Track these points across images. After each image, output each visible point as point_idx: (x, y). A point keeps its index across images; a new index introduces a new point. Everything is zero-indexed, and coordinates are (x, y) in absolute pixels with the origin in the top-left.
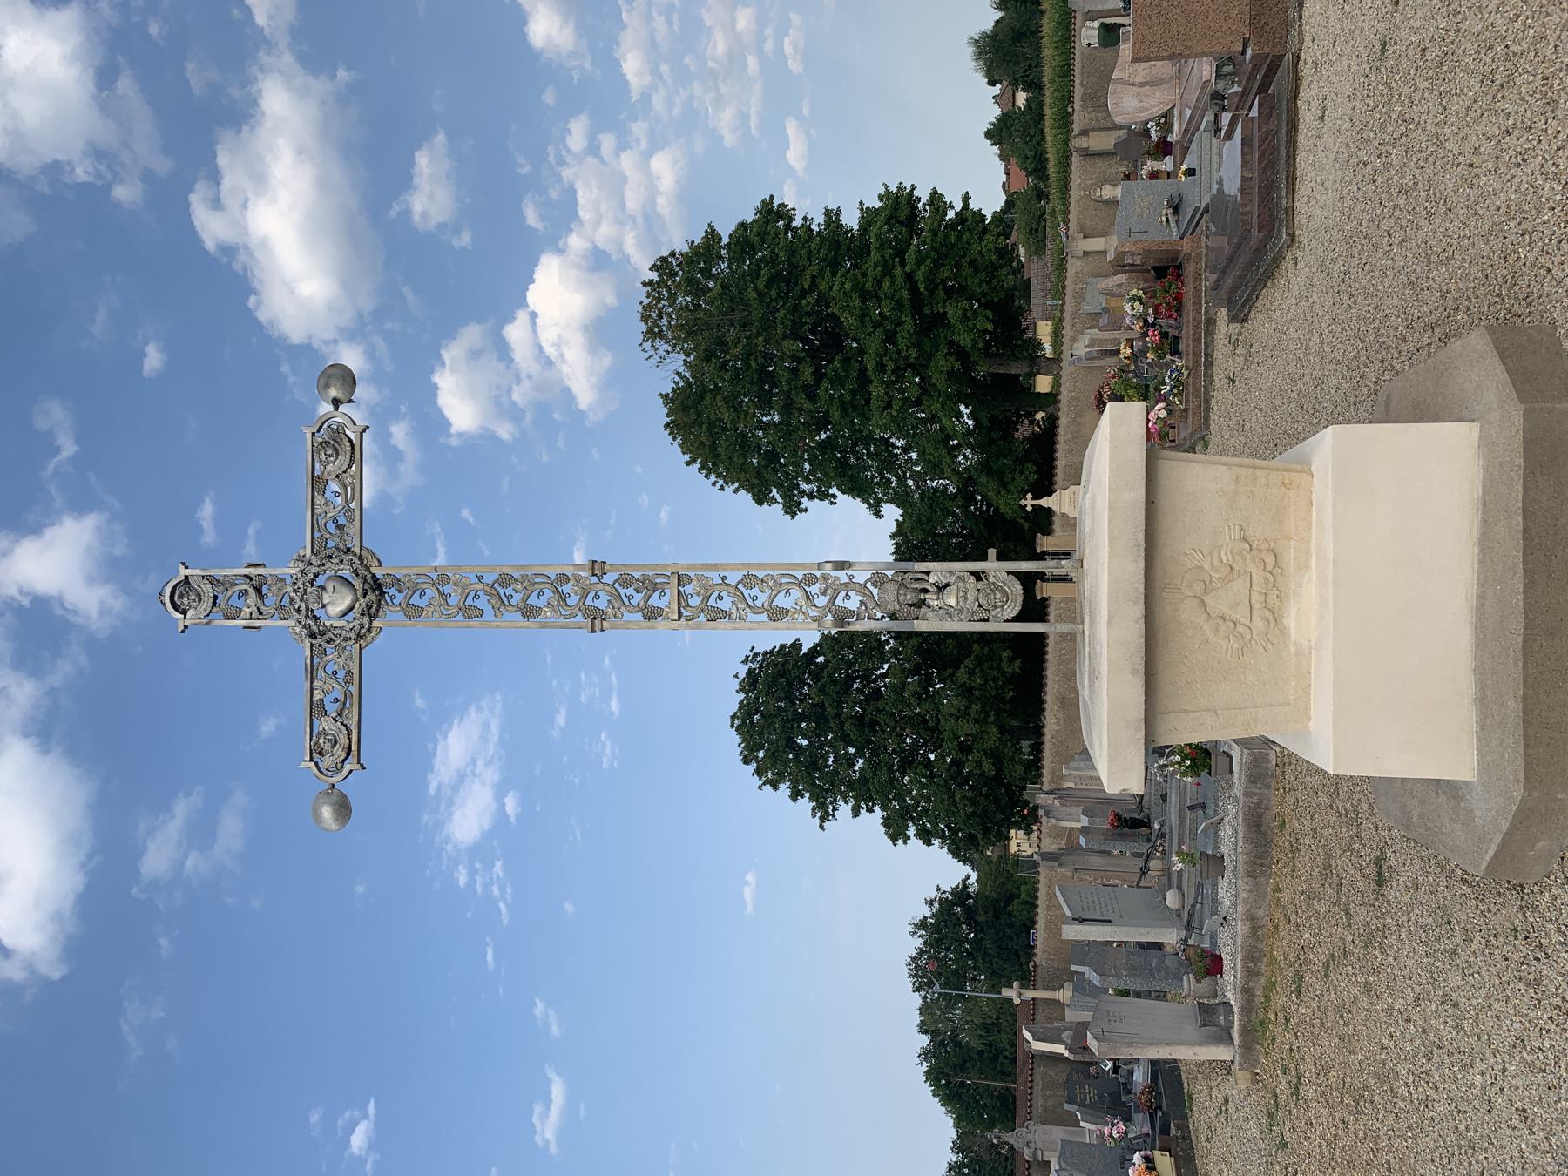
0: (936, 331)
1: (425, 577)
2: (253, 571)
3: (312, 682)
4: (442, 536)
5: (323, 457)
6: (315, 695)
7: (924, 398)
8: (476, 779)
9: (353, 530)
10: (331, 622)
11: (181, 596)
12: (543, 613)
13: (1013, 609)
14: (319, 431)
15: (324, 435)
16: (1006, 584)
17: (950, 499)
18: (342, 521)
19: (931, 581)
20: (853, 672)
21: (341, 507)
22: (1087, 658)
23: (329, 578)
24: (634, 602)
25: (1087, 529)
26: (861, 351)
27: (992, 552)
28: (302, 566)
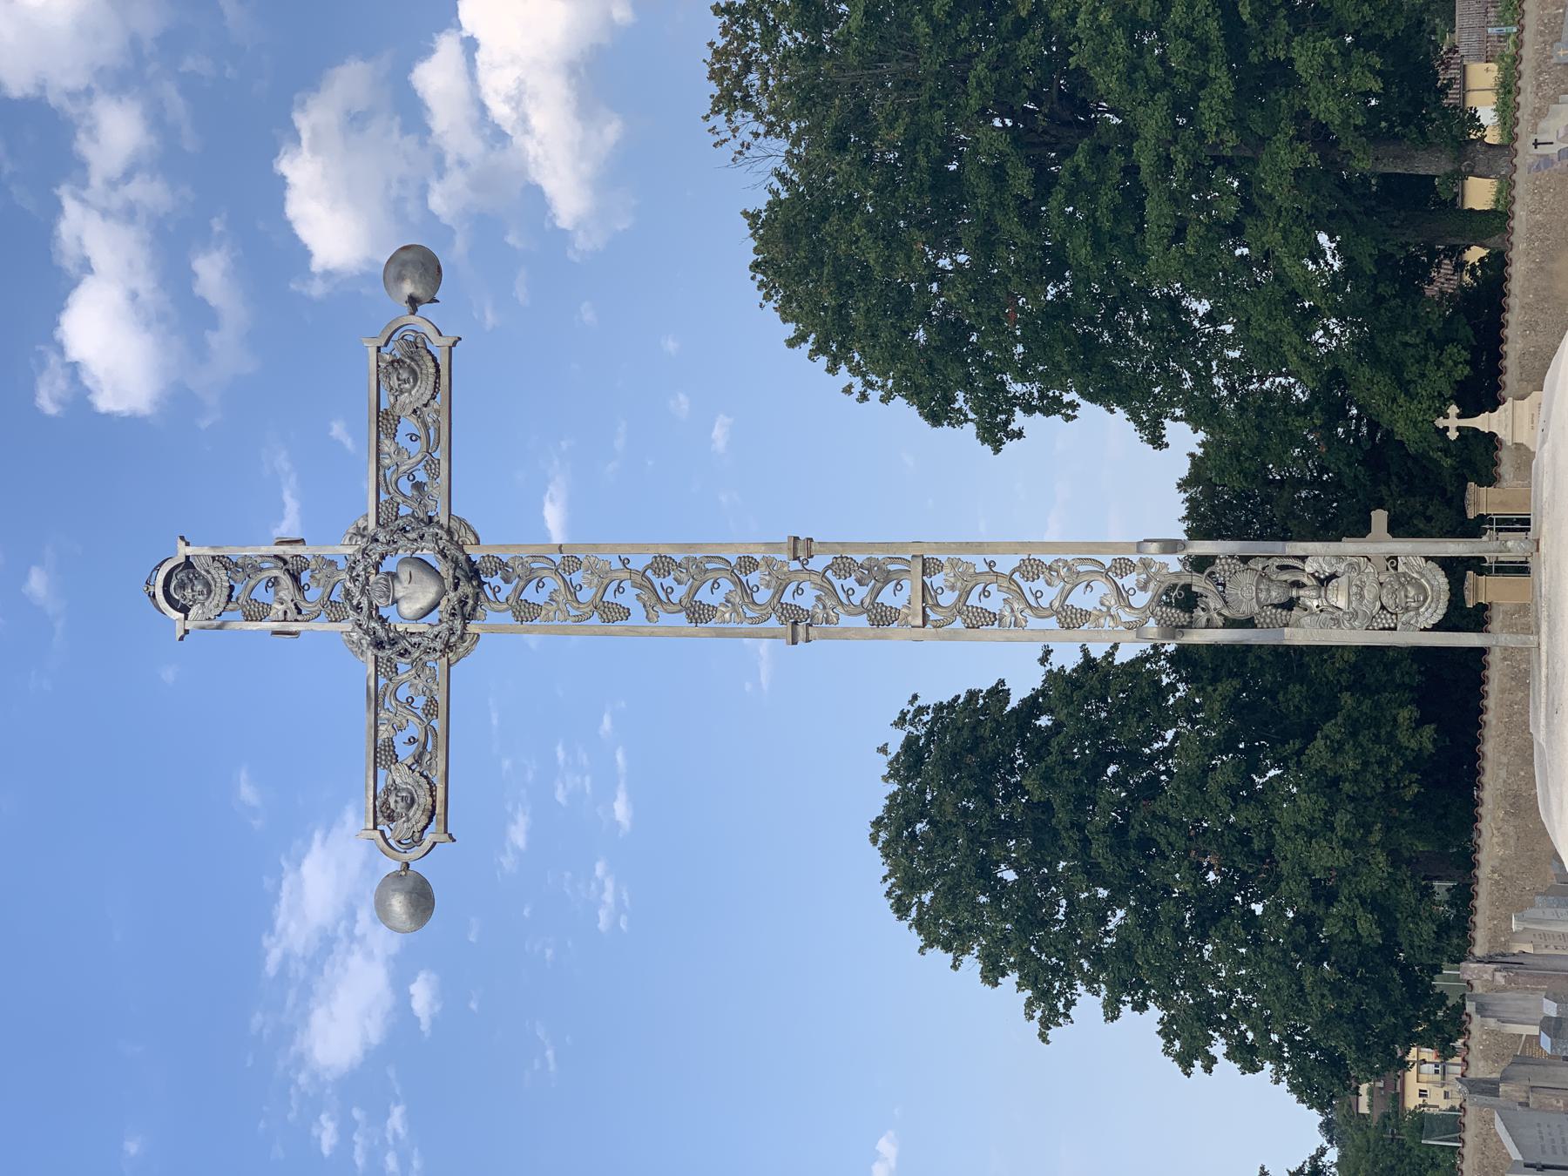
0: (1272, 95)
1: (545, 561)
2: (287, 551)
3: (376, 714)
4: (293, 479)
5: (394, 382)
6: (380, 733)
7: (1249, 222)
8: (355, 947)
9: (437, 490)
10: (407, 626)
11: (182, 586)
12: (719, 614)
13: (1435, 611)
14: (386, 345)
15: (395, 350)
16: (1423, 576)
17: (1299, 414)
18: (421, 476)
19: (1308, 569)
20: (1105, 745)
21: (420, 457)
22: (1544, 684)
23: (404, 561)
24: (856, 600)
25: (1545, 495)
26: (1128, 133)
27: (1379, 518)
28: (362, 543)
